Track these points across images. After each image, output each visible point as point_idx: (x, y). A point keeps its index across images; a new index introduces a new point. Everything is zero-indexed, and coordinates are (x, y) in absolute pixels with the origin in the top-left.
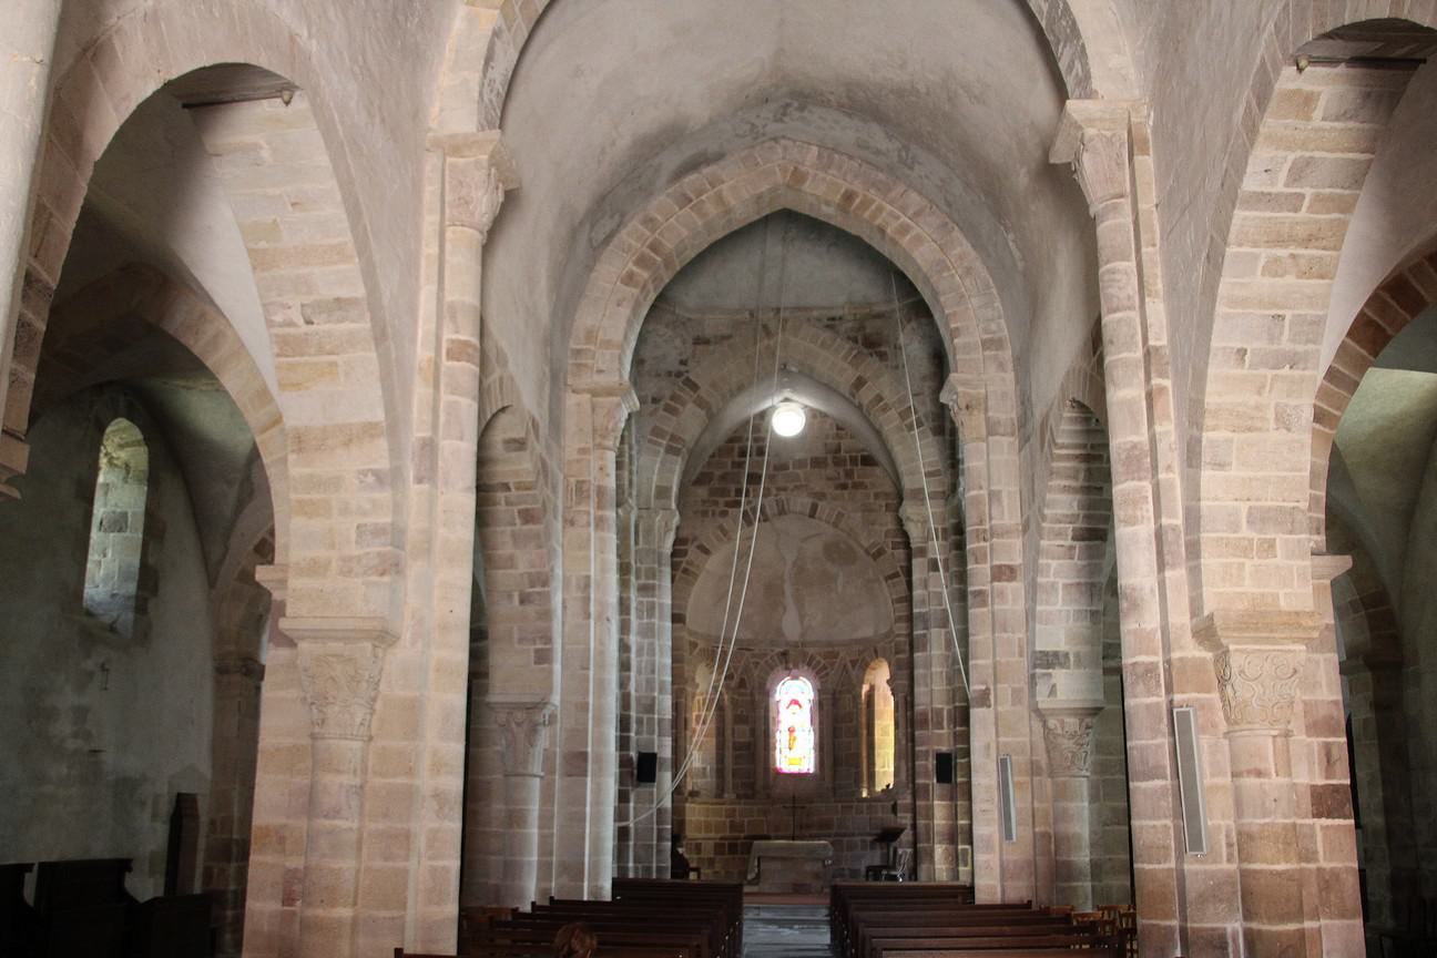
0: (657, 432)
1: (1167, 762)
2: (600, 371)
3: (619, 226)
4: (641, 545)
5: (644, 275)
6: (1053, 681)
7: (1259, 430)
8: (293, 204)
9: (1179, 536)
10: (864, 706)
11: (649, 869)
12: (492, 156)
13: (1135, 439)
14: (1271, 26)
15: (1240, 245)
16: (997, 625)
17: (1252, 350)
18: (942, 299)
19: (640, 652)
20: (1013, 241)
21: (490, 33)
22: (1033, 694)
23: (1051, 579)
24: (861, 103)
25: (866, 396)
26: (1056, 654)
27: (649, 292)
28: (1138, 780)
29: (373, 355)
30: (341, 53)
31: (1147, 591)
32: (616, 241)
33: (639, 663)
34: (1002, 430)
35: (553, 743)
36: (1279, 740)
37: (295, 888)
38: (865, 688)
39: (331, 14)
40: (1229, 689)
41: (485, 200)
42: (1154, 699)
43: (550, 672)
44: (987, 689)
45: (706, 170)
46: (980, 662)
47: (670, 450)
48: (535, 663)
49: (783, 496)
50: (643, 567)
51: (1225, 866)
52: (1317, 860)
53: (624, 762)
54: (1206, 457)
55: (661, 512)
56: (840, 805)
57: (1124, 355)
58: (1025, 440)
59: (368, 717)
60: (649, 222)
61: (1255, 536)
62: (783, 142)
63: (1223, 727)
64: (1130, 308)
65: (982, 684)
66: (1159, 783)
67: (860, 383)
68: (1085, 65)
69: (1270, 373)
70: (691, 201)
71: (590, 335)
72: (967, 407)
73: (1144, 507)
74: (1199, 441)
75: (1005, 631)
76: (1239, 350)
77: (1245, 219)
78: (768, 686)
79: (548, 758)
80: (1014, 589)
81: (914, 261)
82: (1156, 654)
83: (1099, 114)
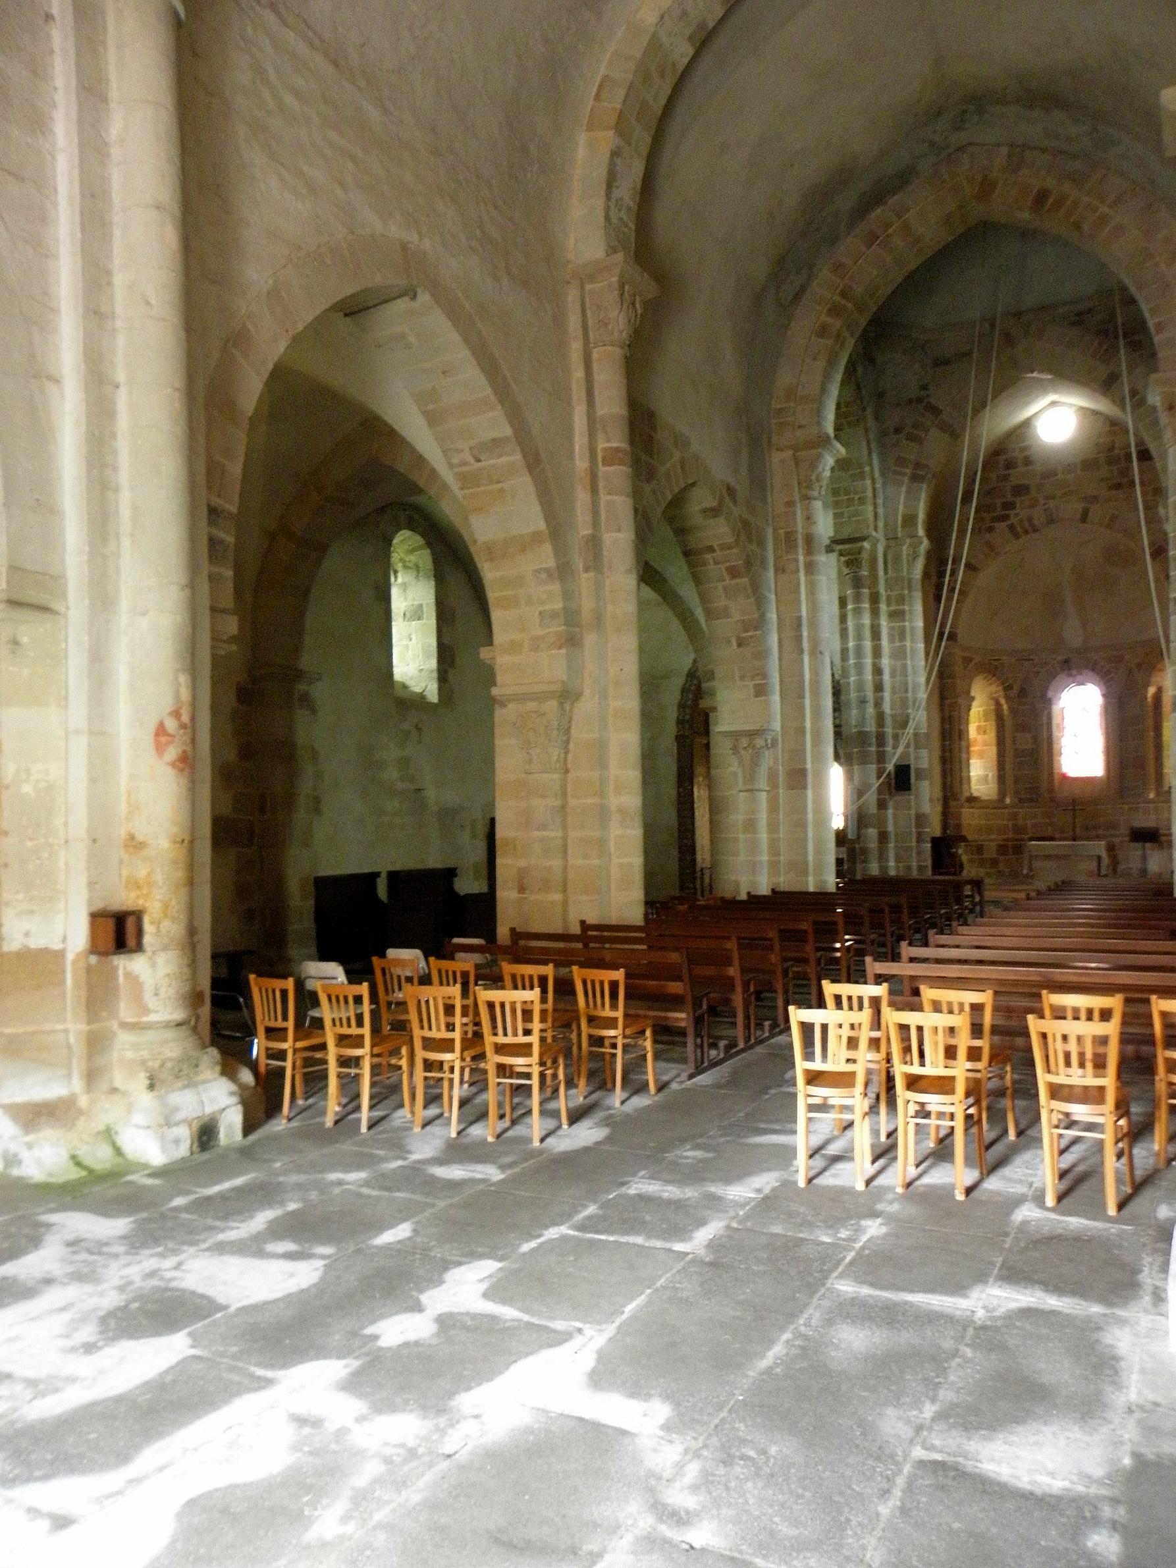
0: (901, 461)
5: (836, 324)
10: (1151, 709)
11: (909, 868)
19: (893, 674)
24: (1040, 94)
29: (527, 479)
33: (893, 684)
35: (776, 762)
38: (1152, 691)
43: (768, 704)
45: (892, 201)
47: (915, 478)
49: (1051, 504)
50: (894, 593)
55: (908, 540)
56: (1126, 807)
60: (838, 268)
62: (970, 149)
71: (790, 393)
78: (1050, 694)
79: (772, 776)
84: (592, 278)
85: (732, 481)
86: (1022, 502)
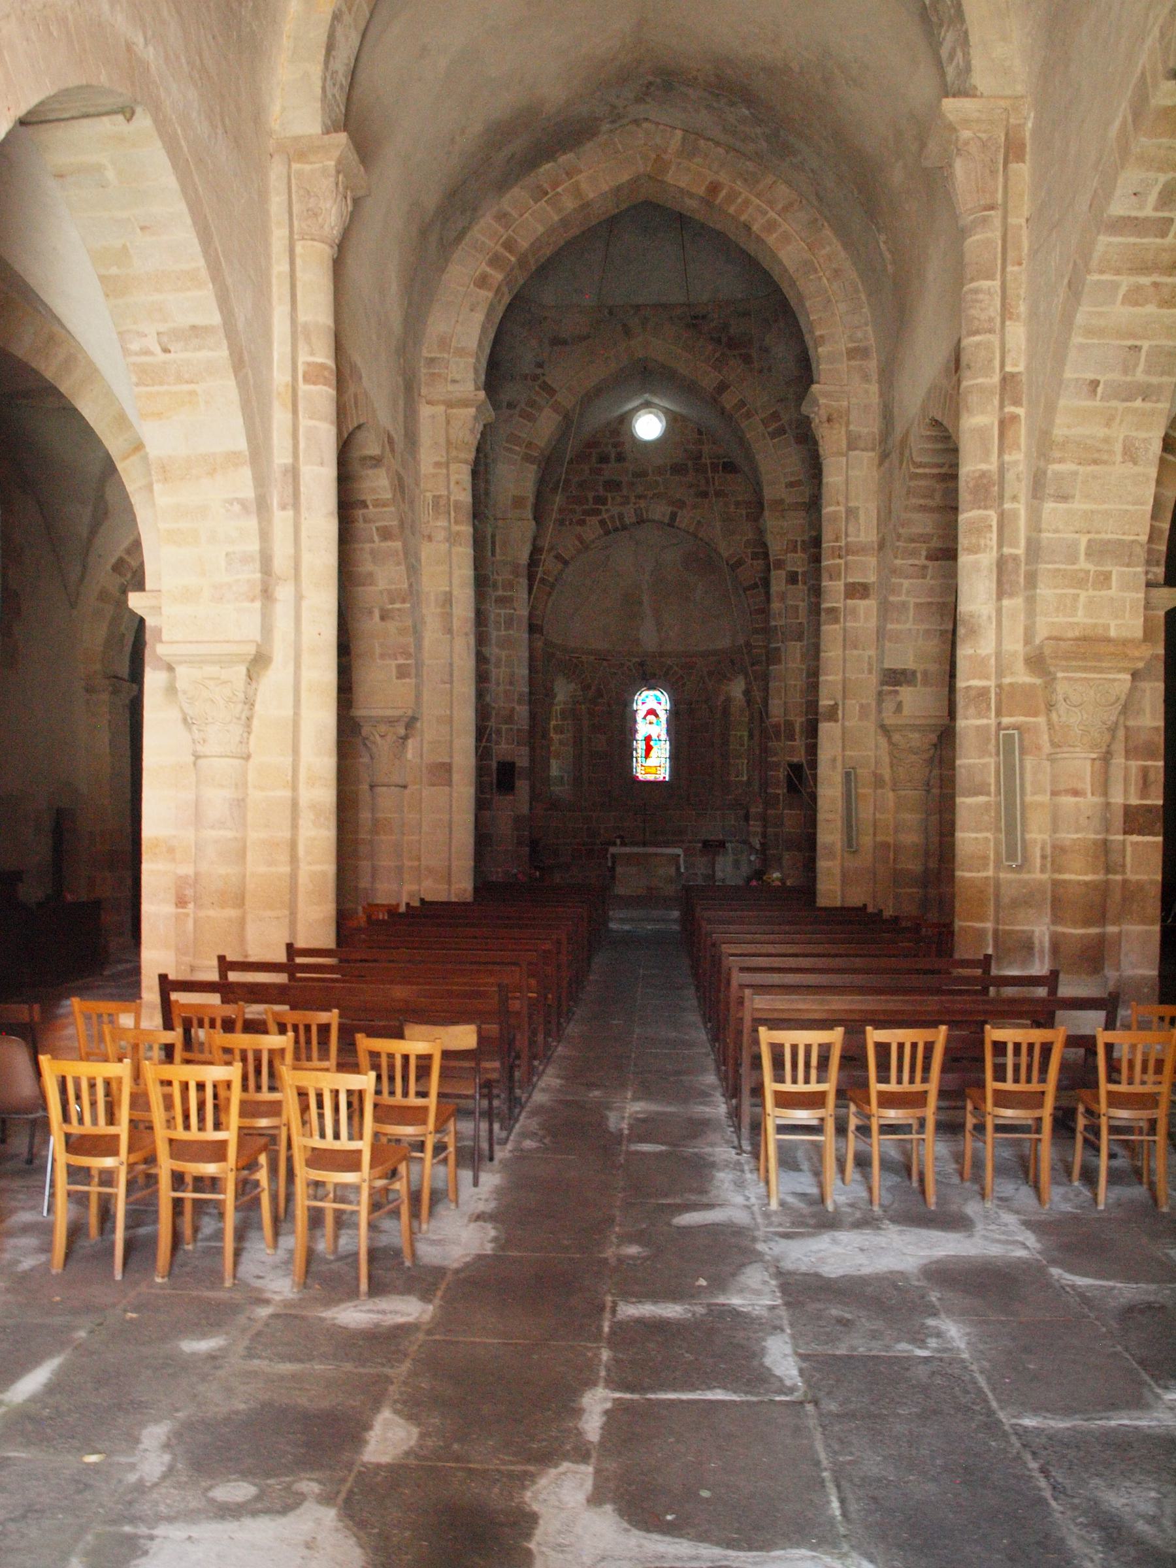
1: (992, 781)
2: (454, 381)
3: (470, 223)
4: (498, 557)
6: (899, 698)
7: (1105, 462)
8: (142, 228)
9: (1018, 565)
12: (339, 162)
13: (984, 467)
14: (1156, 32)
15: (1102, 272)
16: (849, 642)
17: (1106, 383)
18: (808, 304)
20: (884, 243)
21: (330, 17)
22: (880, 711)
23: (903, 598)
25: (729, 400)
26: (904, 672)
27: (503, 294)
28: (964, 795)
29: (231, 383)
30: (178, 58)
31: (985, 618)
32: (467, 239)
34: (862, 445)
36: (1097, 762)
37: (187, 892)
39: (165, 13)
40: (1054, 716)
41: (334, 209)
42: (984, 721)
44: (836, 704)
46: (830, 678)
47: (527, 458)
48: (398, 678)
49: (642, 504)
51: (1038, 875)
52: (1124, 872)
53: (481, 770)
54: (1050, 490)
57: (980, 380)
58: (884, 456)
59: (245, 735)
60: (502, 217)
61: (1091, 567)
62: (645, 125)
63: (1047, 748)
64: (991, 331)
65: (831, 699)
66: (982, 799)
67: (722, 387)
68: (966, 54)
69: (1121, 406)
70: (546, 193)
71: (444, 343)
72: (829, 420)
73: (988, 535)
74: (1045, 473)
75: (856, 647)
76: (1092, 382)
77: (1109, 244)
80: (866, 607)
81: (781, 263)
82: (987, 678)
83: (976, 115)
84: (302, 156)
85: (390, 428)
86: (613, 498)
